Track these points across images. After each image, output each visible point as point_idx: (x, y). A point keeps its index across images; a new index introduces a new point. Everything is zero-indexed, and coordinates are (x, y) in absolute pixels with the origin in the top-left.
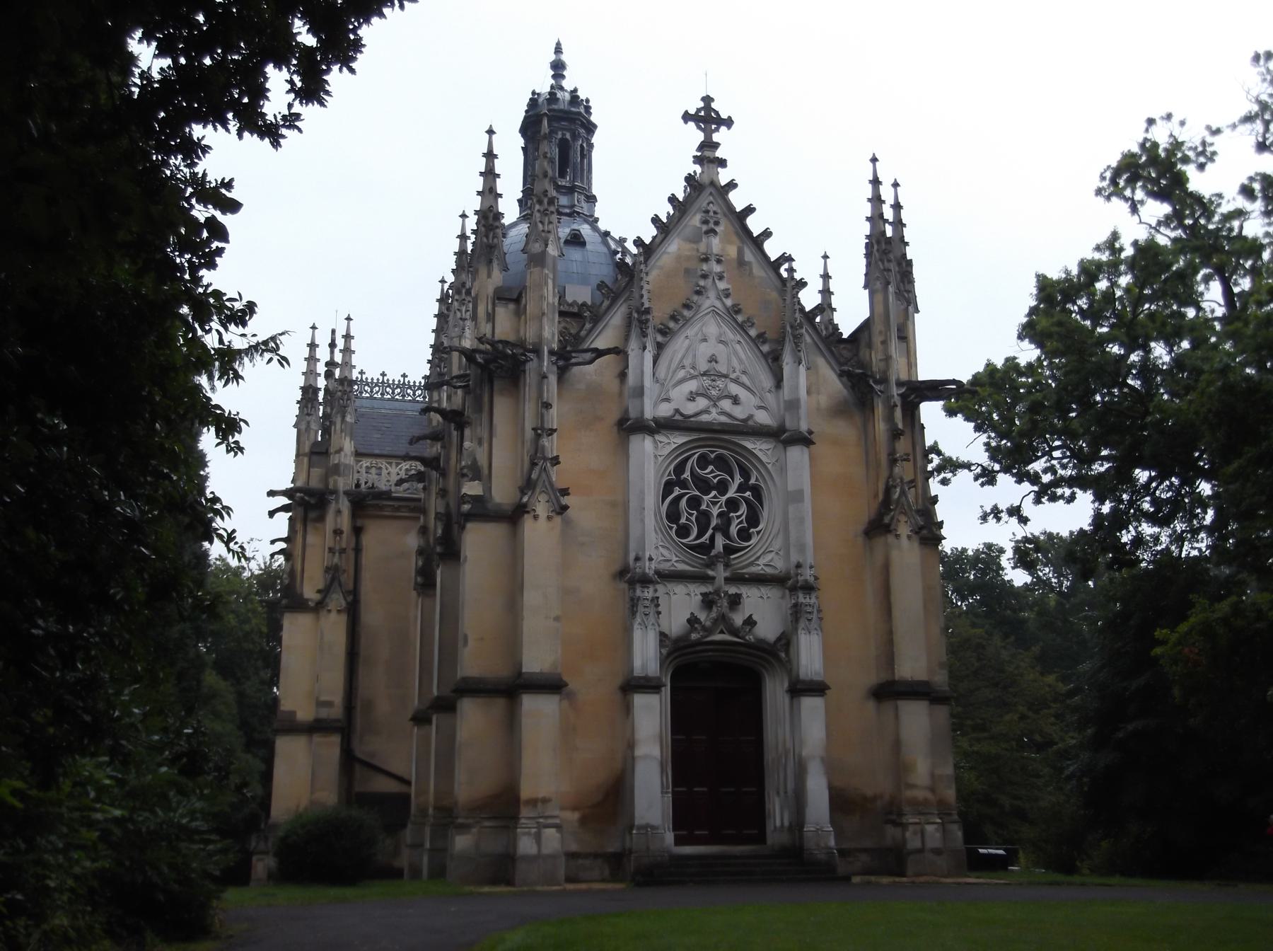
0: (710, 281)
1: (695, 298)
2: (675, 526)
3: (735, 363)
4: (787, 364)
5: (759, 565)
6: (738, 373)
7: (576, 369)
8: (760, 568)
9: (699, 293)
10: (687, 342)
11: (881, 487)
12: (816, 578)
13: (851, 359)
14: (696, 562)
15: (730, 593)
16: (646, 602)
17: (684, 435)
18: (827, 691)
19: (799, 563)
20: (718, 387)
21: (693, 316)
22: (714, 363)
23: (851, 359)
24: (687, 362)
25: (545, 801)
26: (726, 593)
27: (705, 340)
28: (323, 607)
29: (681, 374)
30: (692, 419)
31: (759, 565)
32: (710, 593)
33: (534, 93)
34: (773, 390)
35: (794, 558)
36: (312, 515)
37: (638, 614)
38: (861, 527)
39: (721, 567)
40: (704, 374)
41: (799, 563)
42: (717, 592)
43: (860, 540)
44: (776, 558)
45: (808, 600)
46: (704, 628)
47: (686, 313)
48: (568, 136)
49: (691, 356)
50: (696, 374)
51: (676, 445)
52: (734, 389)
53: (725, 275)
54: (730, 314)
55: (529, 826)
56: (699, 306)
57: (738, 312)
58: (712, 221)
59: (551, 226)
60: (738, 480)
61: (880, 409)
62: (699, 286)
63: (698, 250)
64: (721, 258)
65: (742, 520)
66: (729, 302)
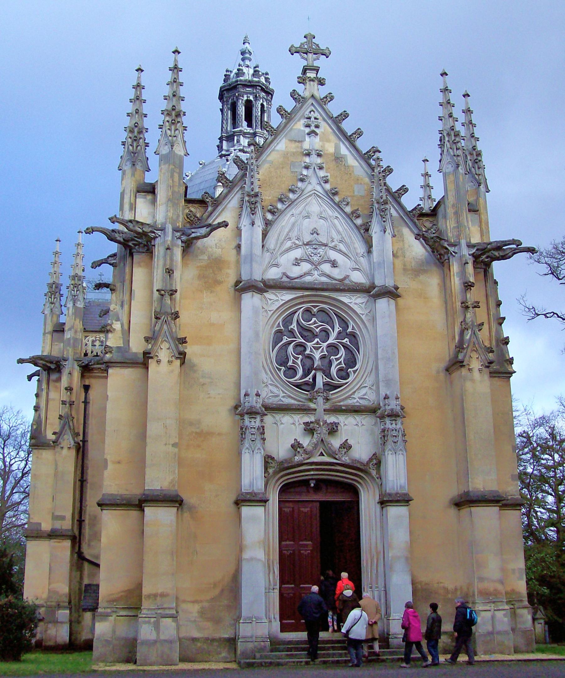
0: (311, 171)
1: (300, 184)
2: (283, 368)
3: (334, 234)
4: (375, 233)
5: (355, 398)
6: (336, 242)
7: (200, 243)
8: (355, 401)
9: (302, 180)
10: (293, 219)
11: (457, 330)
12: (402, 408)
13: (432, 228)
14: (301, 397)
15: (328, 422)
16: (253, 430)
17: (291, 294)
18: (410, 502)
19: (386, 395)
20: (319, 253)
21: (297, 198)
22: (315, 235)
23: (432, 228)
24: (294, 235)
25: (163, 595)
26: (325, 422)
27: (308, 217)
28: (58, 445)
29: (288, 244)
30: (296, 280)
31: (355, 398)
32: (312, 422)
33: (227, 71)
34: (366, 254)
35: (383, 391)
36: (54, 376)
37: (246, 440)
38: (443, 365)
39: (320, 400)
40: (307, 244)
41: (386, 395)
42: (317, 422)
43: (442, 375)
44: (369, 392)
45: (394, 425)
46: (306, 452)
47: (291, 196)
48: (251, 98)
49: (296, 229)
50: (301, 244)
51: (284, 302)
52: (333, 255)
53: (324, 165)
54: (328, 194)
55: (149, 616)
56: (303, 191)
57: (335, 194)
58: (313, 125)
59: (177, 132)
60: (337, 328)
61: (455, 268)
62: (302, 175)
63: (302, 147)
64: (321, 152)
65: (341, 362)
66: (328, 187)
